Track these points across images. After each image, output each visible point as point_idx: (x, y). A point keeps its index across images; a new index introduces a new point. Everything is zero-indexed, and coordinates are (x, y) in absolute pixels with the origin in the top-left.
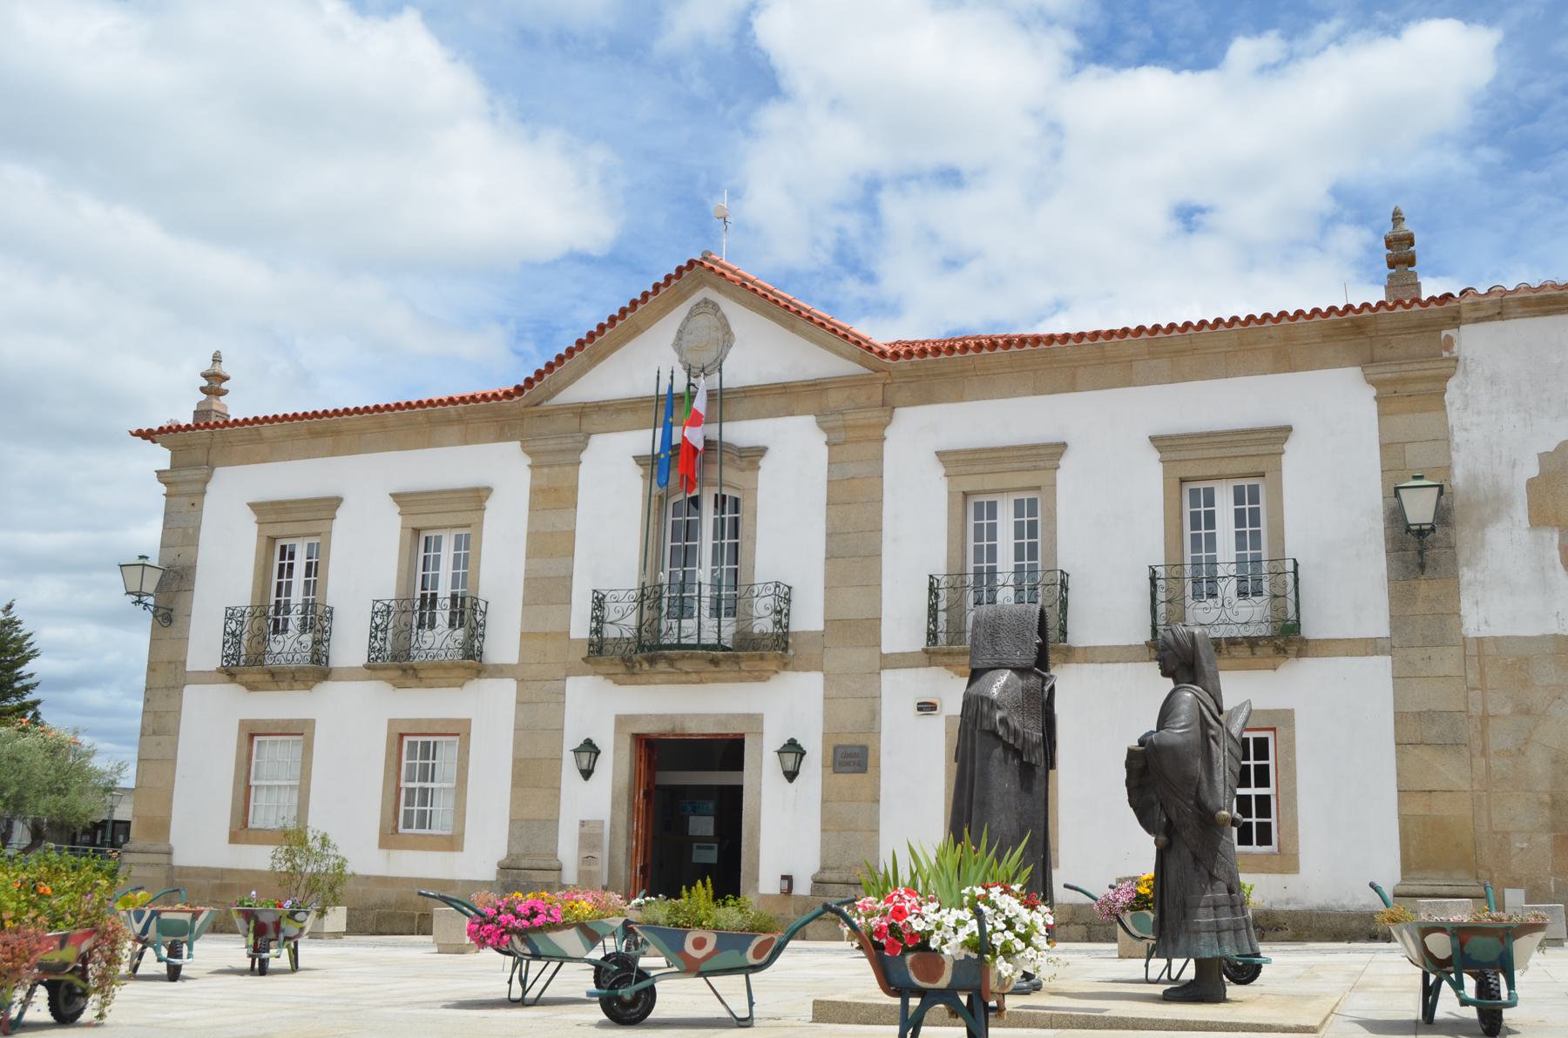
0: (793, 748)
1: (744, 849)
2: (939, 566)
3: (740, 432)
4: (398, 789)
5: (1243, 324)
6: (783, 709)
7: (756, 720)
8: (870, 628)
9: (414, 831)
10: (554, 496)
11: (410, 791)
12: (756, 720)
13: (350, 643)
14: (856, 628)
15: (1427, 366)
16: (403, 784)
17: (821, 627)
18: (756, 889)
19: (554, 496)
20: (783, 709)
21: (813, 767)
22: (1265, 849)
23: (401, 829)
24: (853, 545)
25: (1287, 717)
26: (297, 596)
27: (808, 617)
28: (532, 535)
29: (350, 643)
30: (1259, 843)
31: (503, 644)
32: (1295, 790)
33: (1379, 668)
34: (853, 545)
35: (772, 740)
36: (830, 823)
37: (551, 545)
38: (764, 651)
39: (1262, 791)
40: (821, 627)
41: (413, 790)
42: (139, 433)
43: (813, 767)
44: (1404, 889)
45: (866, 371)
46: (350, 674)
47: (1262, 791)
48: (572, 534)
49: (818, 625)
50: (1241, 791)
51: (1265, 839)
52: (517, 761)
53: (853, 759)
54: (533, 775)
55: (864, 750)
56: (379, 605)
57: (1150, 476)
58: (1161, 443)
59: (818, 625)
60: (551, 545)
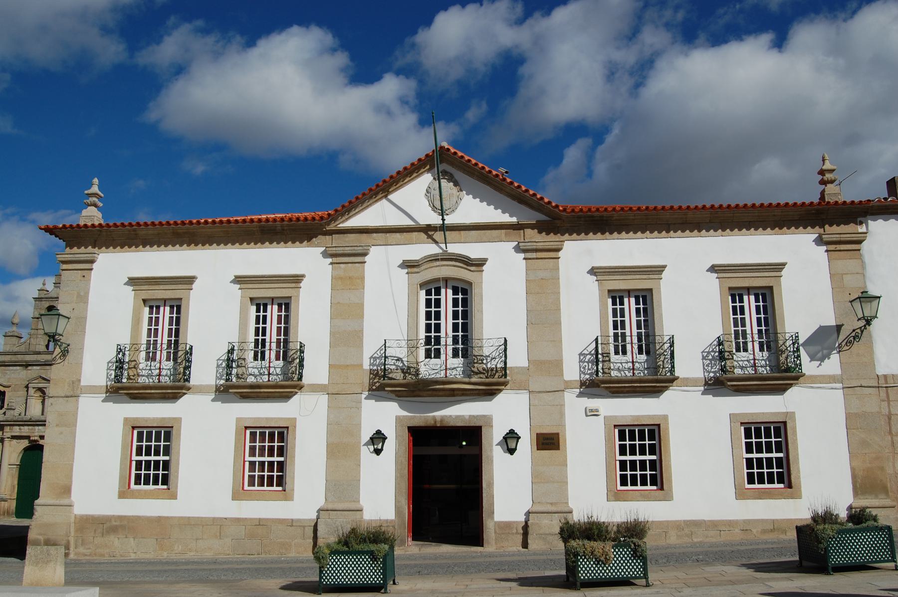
1: (484, 495)
3: (472, 250)
4: (244, 461)
6: (505, 413)
7: (488, 419)
8: (557, 365)
11: (252, 464)
12: (488, 419)
18: (493, 518)
20: (505, 413)
21: (525, 445)
22: (147, 487)
23: (246, 487)
24: (543, 314)
26: (272, 336)
27: (518, 358)
29: (690, 363)
30: (631, 485)
31: (316, 370)
32: (798, 454)
33: (837, 396)
34: (543, 314)
35: (497, 433)
36: (537, 478)
37: (347, 313)
38: (489, 384)
41: (264, 462)
43: (525, 445)
46: (201, 390)
48: (361, 306)
52: (328, 445)
53: (548, 442)
54: (341, 451)
55: (539, 448)
57: (713, 285)
60: (347, 313)
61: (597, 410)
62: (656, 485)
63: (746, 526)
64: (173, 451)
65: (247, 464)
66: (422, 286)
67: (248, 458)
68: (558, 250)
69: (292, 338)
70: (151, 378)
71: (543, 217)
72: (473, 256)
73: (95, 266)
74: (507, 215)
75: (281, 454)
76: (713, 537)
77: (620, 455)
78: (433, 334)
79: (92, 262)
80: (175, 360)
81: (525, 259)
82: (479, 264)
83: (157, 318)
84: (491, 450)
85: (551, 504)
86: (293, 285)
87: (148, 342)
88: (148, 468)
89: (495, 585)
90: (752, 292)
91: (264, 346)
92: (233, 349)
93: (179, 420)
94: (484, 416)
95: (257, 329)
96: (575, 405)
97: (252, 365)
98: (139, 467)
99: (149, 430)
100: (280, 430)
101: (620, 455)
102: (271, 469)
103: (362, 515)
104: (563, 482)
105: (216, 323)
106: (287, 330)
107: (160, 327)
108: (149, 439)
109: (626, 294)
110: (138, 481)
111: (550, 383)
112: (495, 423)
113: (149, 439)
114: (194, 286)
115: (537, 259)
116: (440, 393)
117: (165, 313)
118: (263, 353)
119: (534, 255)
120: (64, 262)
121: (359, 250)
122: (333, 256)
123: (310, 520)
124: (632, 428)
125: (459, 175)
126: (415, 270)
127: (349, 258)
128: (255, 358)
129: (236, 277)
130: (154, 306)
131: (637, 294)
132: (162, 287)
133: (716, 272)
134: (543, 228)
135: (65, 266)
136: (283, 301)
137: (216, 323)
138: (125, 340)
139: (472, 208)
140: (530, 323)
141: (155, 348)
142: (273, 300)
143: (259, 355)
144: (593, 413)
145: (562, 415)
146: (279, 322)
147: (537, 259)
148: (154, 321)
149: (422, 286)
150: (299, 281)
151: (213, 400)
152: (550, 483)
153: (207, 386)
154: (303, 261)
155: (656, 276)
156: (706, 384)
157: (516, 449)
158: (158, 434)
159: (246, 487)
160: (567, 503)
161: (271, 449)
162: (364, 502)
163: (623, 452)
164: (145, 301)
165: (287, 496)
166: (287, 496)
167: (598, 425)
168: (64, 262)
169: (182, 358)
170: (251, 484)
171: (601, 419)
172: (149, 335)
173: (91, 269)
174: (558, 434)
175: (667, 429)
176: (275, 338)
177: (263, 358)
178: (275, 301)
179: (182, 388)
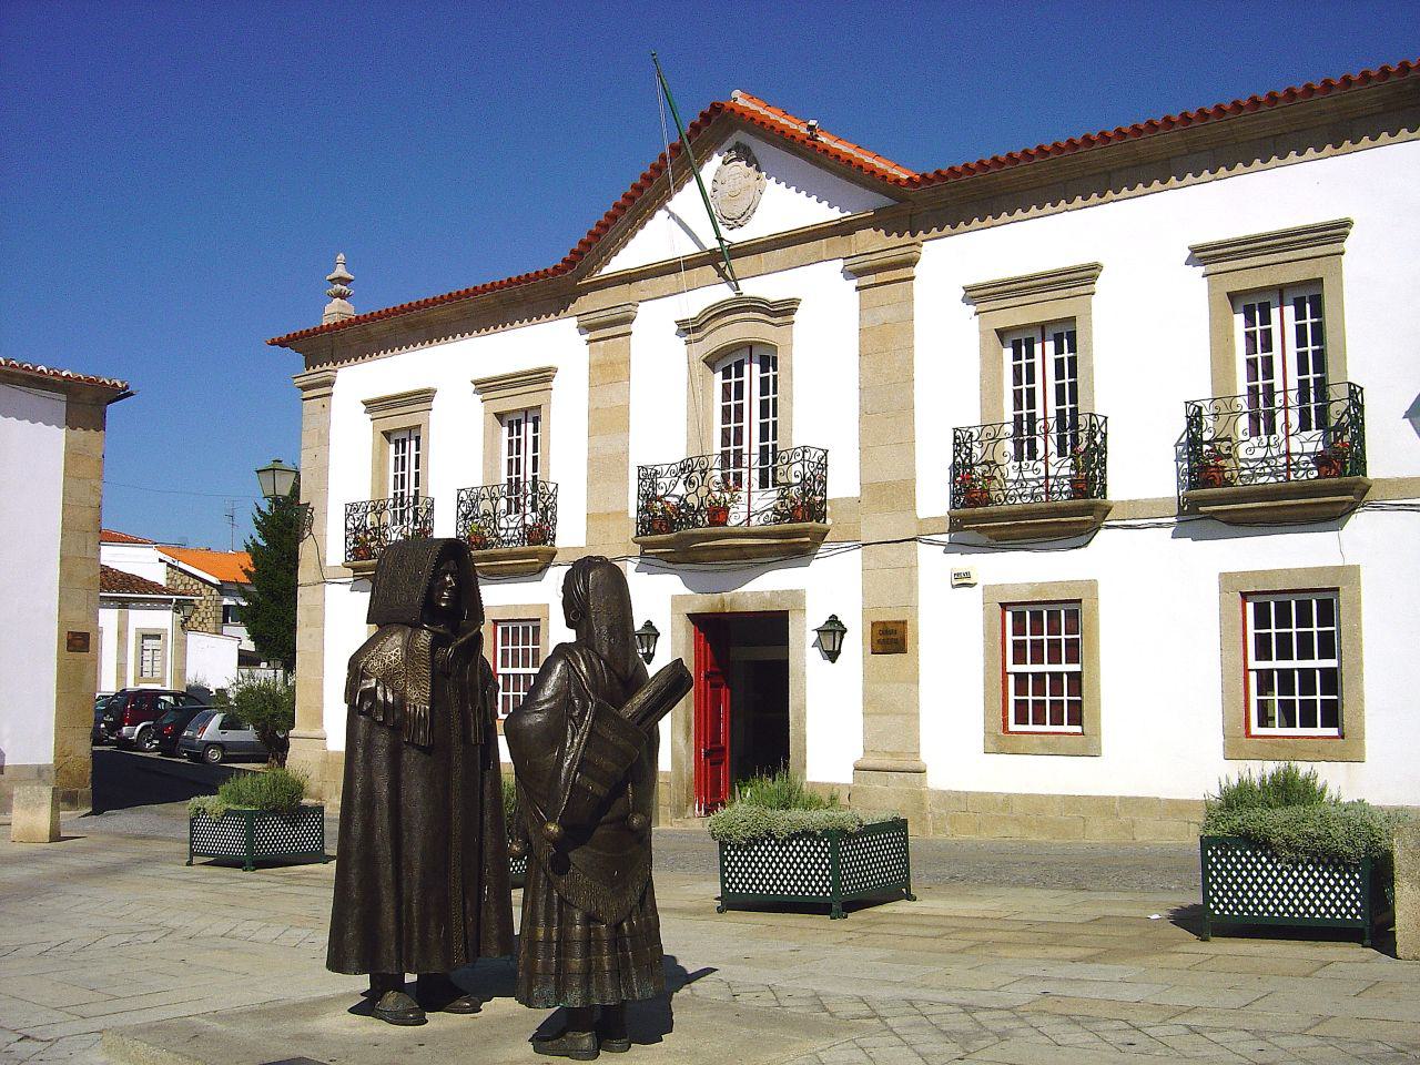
0: (833, 630)
2: (1202, 390)
3: (765, 286)
4: (1005, 674)
5: (553, 275)
6: (824, 588)
7: (798, 596)
9: (1277, 731)
10: (610, 374)
11: (1021, 678)
13: (1143, 468)
14: (892, 491)
15: (901, 257)
16: (1011, 667)
17: (856, 493)
19: (610, 374)
25: (1092, 585)
26: (752, 443)
28: (593, 412)
29: (1143, 468)
36: (874, 706)
37: (609, 420)
39: (1075, 668)
40: (856, 493)
42: (273, 343)
44: (865, 764)
45: (892, 202)
46: (1140, 516)
47: (1075, 668)
49: (854, 491)
50: (1332, 663)
51: (1076, 719)
53: (890, 639)
56: (463, 494)
57: (1194, 290)
58: (1203, 255)
59: (854, 491)
60: (609, 420)
61: (967, 575)
62: (1335, 725)
63: (1002, 806)
64: (1345, 644)
65: (1253, 676)
66: (711, 362)
67: (1253, 664)
68: (912, 263)
69: (1332, 377)
70: (1038, 490)
71: (883, 201)
72: (772, 298)
73: (634, 327)
74: (837, 209)
75: (1327, 652)
76: (1098, 834)
77: (1258, 658)
78: (732, 448)
79: (330, 384)
80: (401, 523)
81: (858, 288)
82: (784, 310)
83: (1031, 367)
84: (803, 654)
85: (892, 754)
86: (542, 386)
87: (1253, 391)
88: (1286, 687)
89: (1351, 957)
90: (1289, 297)
91: (1270, 400)
92: (1199, 414)
93: (1092, 585)
94: (792, 591)
95: (725, 433)
96: (935, 563)
97: (1249, 449)
98: (1021, 688)
99: (525, 624)
100: (1322, 596)
101: (1258, 658)
102: (1308, 687)
103: (922, 783)
104: (912, 715)
105: (1156, 362)
106: (1320, 358)
107: (1038, 385)
108: (1284, 621)
109: (1274, 299)
110: (1021, 719)
111: (893, 527)
112: (809, 603)
113: (1284, 621)
114: (434, 404)
115: (877, 285)
116: (726, 554)
117: (1284, 321)
118: (1271, 417)
119: (871, 279)
120: (305, 388)
121: (618, 314)
122: (858, 273)
123: (1177, 808)
124: (1038, 608)
125: (759, 147)
126: (698, 335)
127: (609, 328)
128: (1255, 432)
129: (1194, 250)
130: (1254, 304)
131: (1298, 295)
132: (401, 410)
133: (1204, 261)
134: (883, 221)
135: (307, 394)
136: (1306, 294)
137: (1156, 362)
138: (1202, 390)
139: (785, 206)
140: (864, 413)
141: (1032, 430)
142: (1042, 327)
143: (1263, 421)
144: (962, 581)
145: (912, 585)
146: (1301, 341)
147: (877, 285)
148: (1024, 374)
149: (711, 362)
150: (548, 379)
151: (1174, 536)
152: (891, 712)
153: (1153, 503)
154: (550, 342)
155: (1084, 290)
156: (1181, 512)
157: (839, 652)
158: (1304, 608)
159: (1255, 730)
160: (917, 754)
161: (1305, 640)
162: (928, 755)
163: (1263, 652)
164: (1002, 334)
165: (1090, 749)
166: (1090, 749)
167: (972, 600)
168: (305, 388)
169: (1087, 451)
170: (1264, 720)
171: (977, 592)
172: (1252, 376)
173: (330, 395)
174: (905, 622)
175: (1095, 609)
176: (1293, 380)
177: (1271, 430)
178: (1050, 333)
179: (1089, 510)
